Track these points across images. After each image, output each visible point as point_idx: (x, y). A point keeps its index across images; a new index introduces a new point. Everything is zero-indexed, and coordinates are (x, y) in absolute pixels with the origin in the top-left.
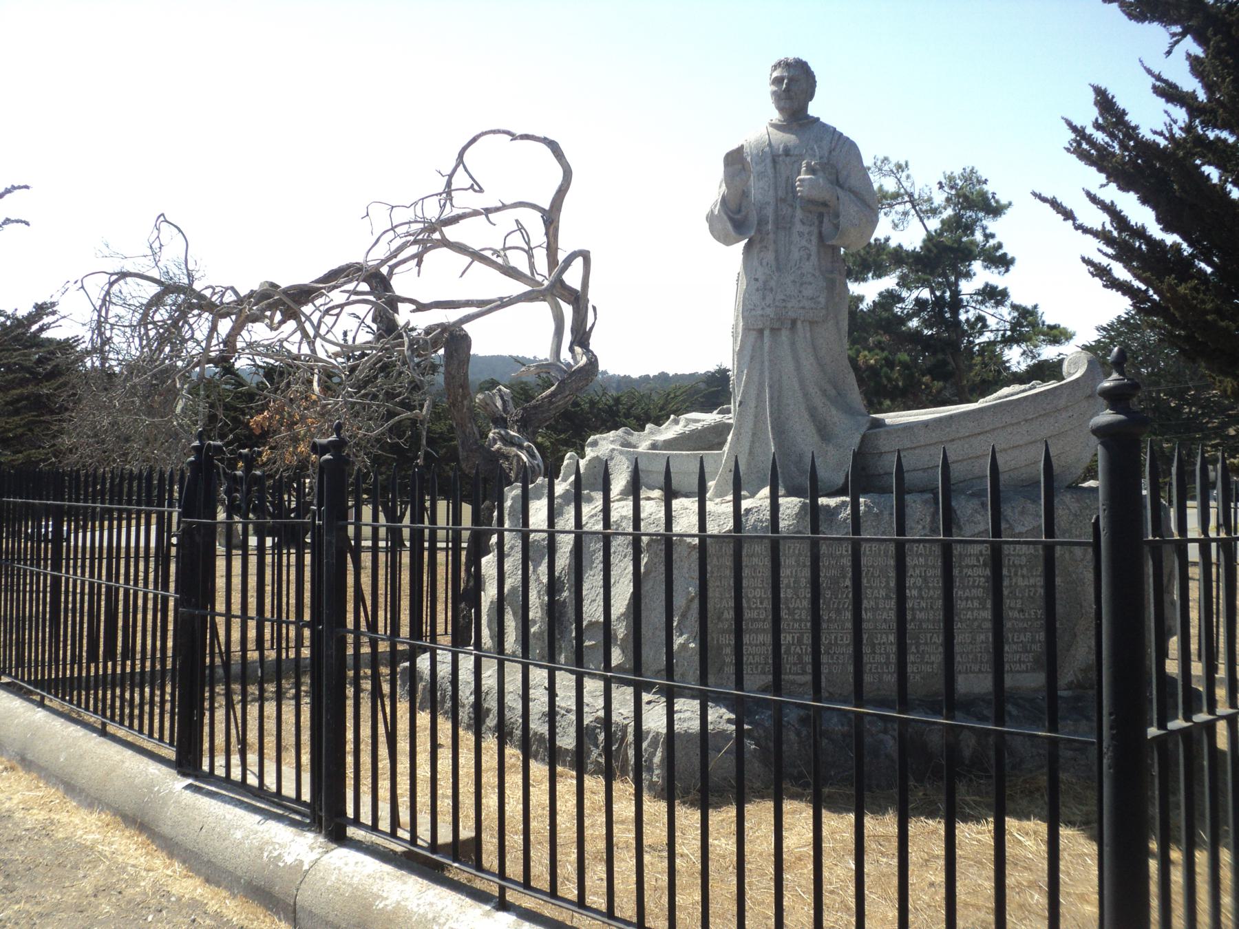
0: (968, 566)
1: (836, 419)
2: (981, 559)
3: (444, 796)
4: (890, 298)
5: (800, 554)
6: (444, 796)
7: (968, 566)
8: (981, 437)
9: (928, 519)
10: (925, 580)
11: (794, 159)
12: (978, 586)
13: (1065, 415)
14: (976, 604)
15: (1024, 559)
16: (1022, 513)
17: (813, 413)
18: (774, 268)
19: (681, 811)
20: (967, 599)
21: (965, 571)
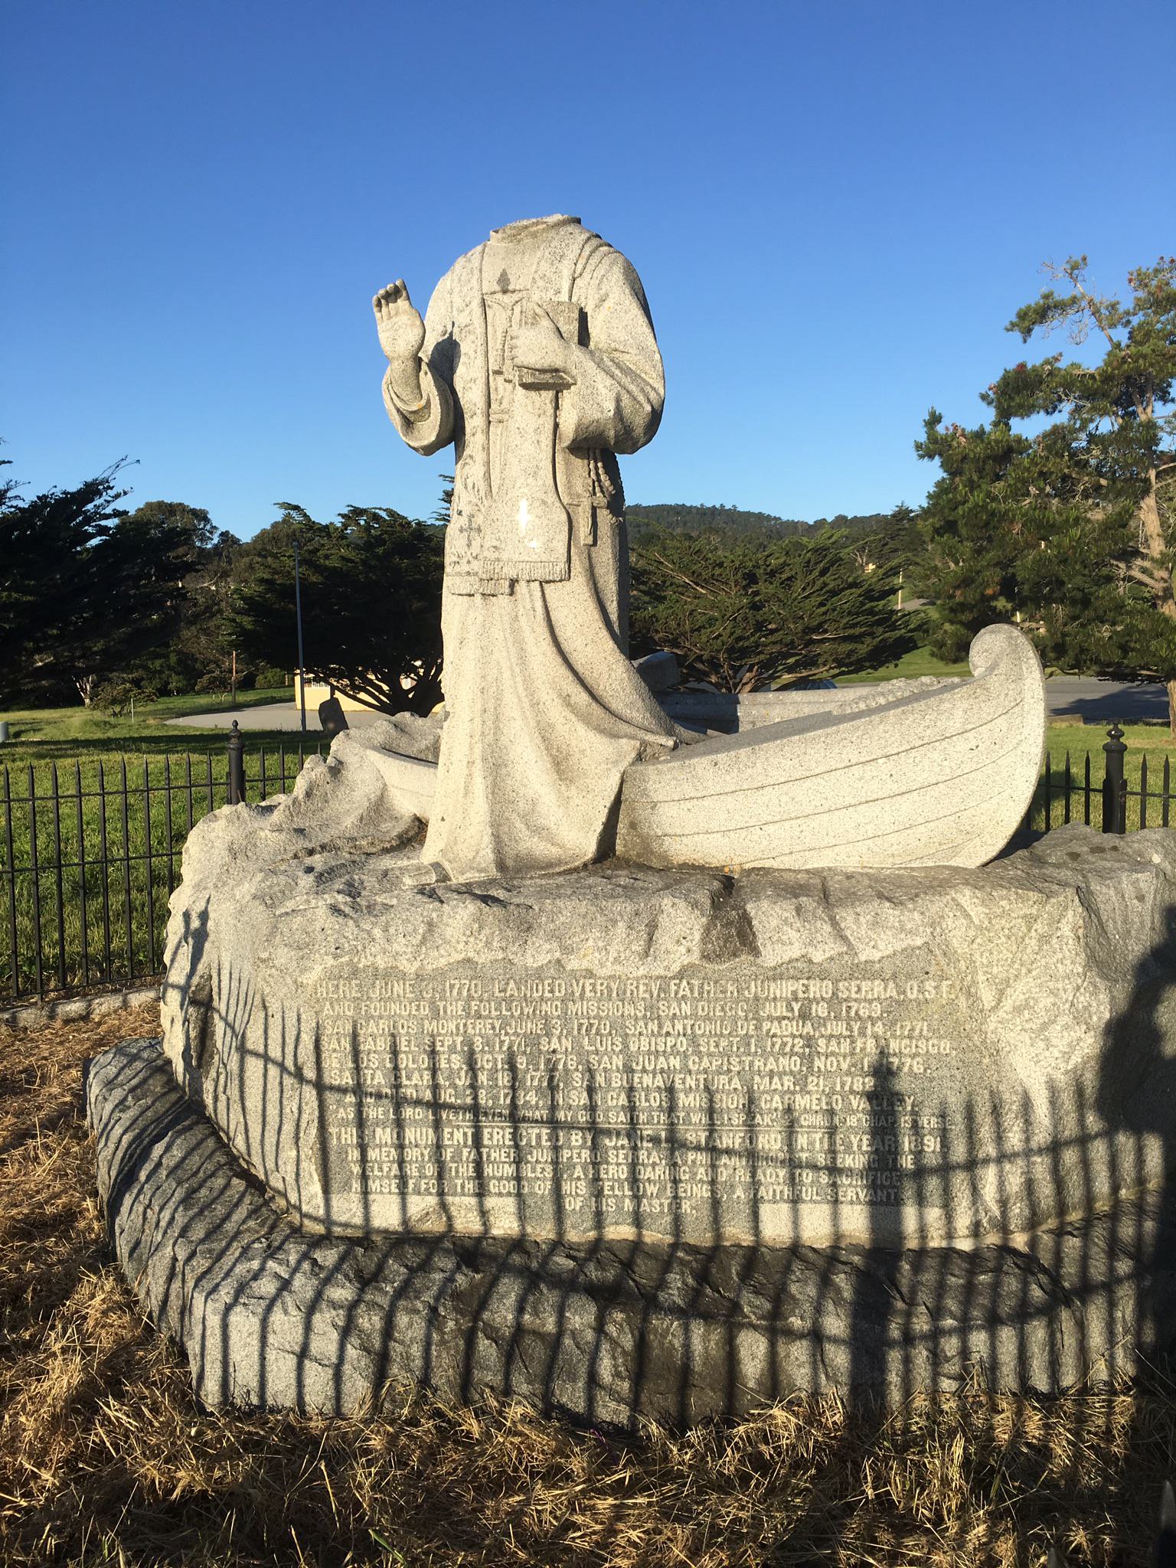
0: (771, 1018)
1: (585, 745)
2: (796, 1007)
3: (344, 1123)
4: (1057, 438)
5: (470, 998)
6: (344, 1123)
7: (771, 1018)
8: (808, 783)
9: (697, 936)
10: (694, 1040)
11: (516, 297)
12: (792, 1054)
13: (961, 745)
14: (788, 1082)
15: (877, 1009)
16: (875, 924)
17: (545, 735)
18: (482, 493)
19: (288, 1400)
20: (771, 1074)
21: (766, 1026)
